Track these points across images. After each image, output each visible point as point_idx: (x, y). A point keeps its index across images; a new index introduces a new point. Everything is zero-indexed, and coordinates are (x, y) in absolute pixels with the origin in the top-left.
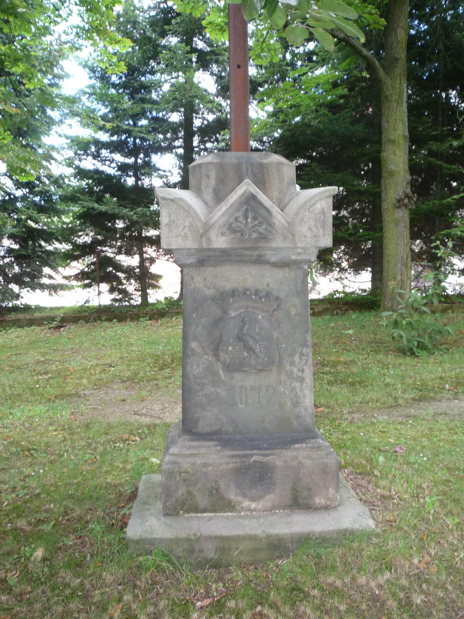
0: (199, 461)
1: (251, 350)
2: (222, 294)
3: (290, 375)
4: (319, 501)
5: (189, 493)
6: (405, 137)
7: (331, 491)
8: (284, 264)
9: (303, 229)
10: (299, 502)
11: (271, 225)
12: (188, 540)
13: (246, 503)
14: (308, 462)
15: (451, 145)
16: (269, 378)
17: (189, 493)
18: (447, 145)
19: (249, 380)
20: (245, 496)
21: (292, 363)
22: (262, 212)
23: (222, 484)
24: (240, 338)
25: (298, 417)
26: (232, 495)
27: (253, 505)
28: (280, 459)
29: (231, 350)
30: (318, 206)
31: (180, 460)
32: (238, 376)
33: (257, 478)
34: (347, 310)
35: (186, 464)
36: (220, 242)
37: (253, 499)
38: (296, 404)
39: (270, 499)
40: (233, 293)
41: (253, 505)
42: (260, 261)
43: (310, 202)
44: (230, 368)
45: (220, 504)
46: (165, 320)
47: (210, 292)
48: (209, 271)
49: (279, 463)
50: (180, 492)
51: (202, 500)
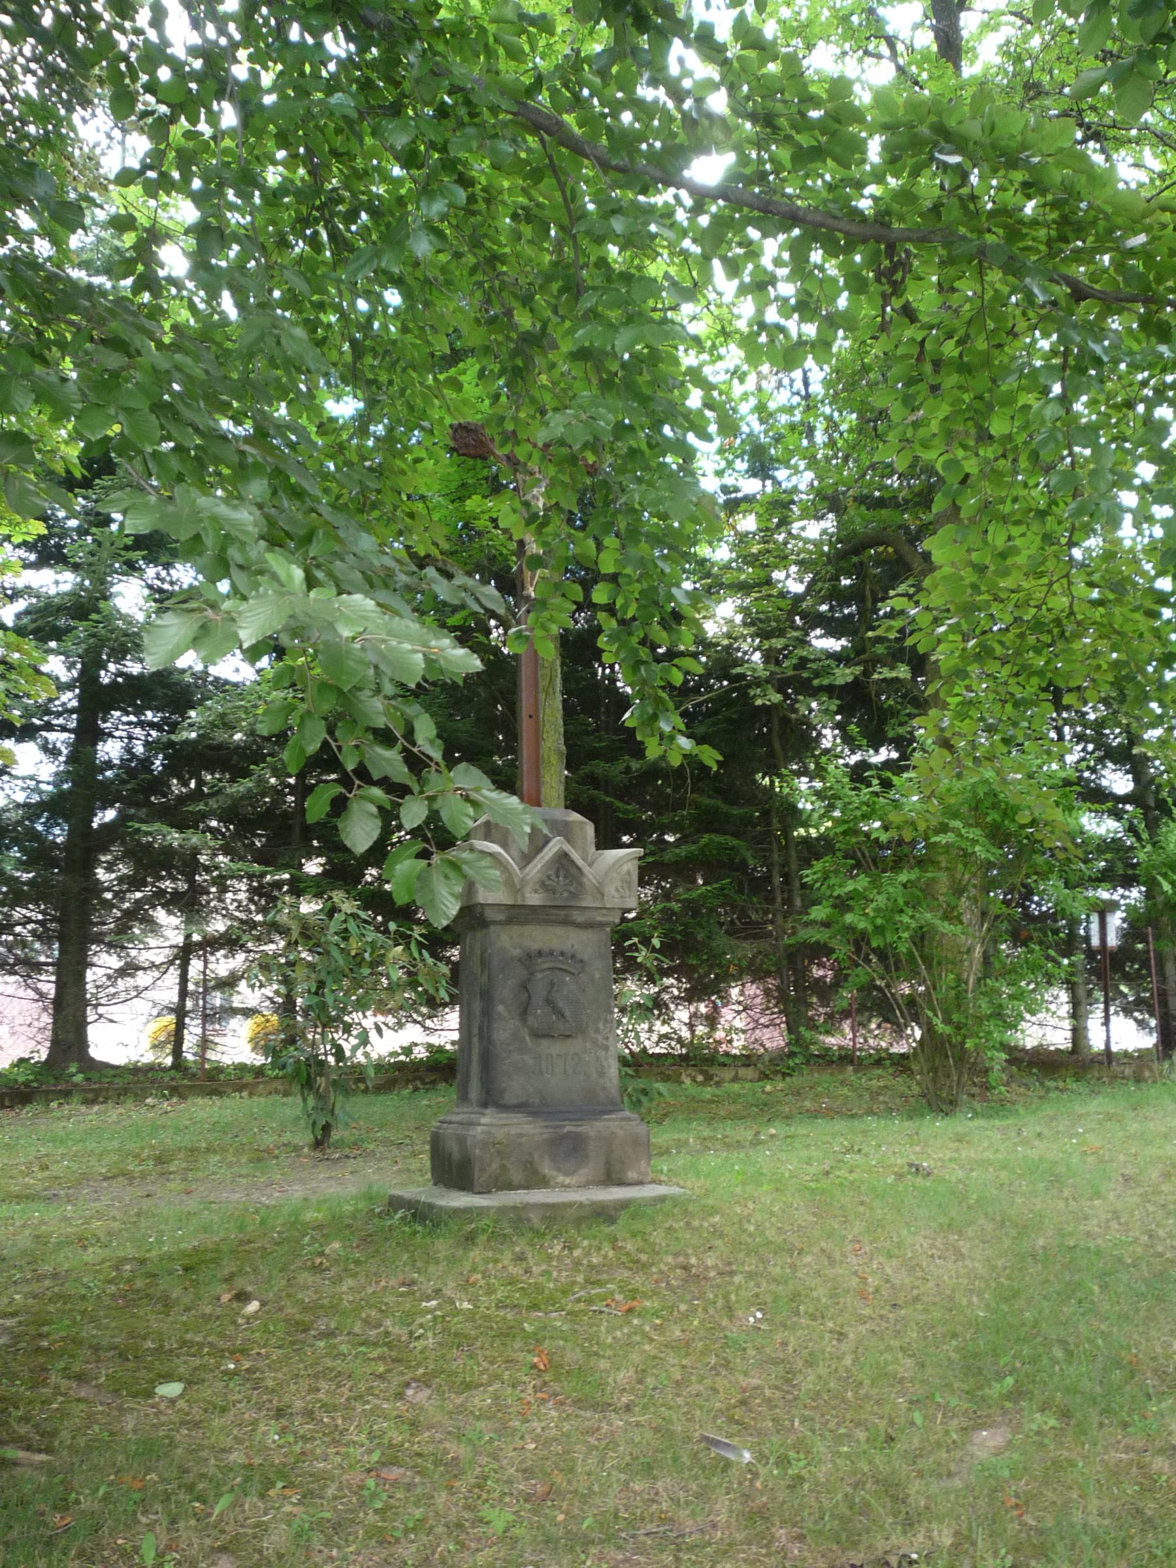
0: (513, 1131)
1: (560, 1014)
2: (529, 956)
3: (595, 1043)
4: (632, 1175)
5: (503, 1167)
6: (560, 753)
7: (643, 1164)
8: (589, 926)
9: (610, 890)
10: (611, 1178)
11: (581, 884)
12: (515, 1208)
13: (560, 1178)
14: (620, 1132)
15: (628, 768)
16: (574, 1046)
17: (503, 1167)
18: (621, 766)
19: (554, 1048)
20: (559, 1170)
21: (597, 1031)
22: (573, 871)
23: (536, 1156)
24: (549, 1002)
25: (604, 1089)
26: (547, 1170)
27: (567, 1181)
28: (592, 1129)
29: (539, 1012)
30: (625, 868)
31: (494, 1130)
32: (544, 1043)
33: (570, 1149)
34: (433, 1082)
35: (500, 1134)
36: (534, 899)
37: (567, 1174)
38: (602, 1074)
39: (584, 1174)
40: (540, 953)
41: (567, 1181)
42: (567, 922)
43: (619, 862)
44: (537, 1035)
45: (536, 1180)
46: (27, 1111)
47: (517, 952)
48: (515, 930)
49: (592, 1134)
50: (494, 1166)
51: (516, 1176)
